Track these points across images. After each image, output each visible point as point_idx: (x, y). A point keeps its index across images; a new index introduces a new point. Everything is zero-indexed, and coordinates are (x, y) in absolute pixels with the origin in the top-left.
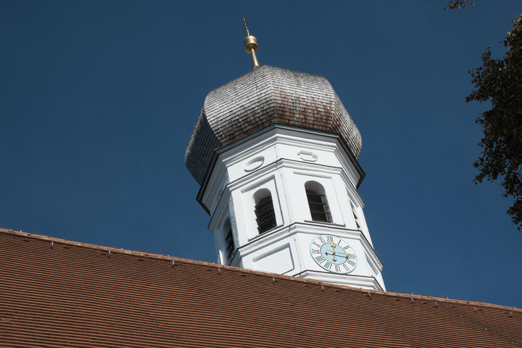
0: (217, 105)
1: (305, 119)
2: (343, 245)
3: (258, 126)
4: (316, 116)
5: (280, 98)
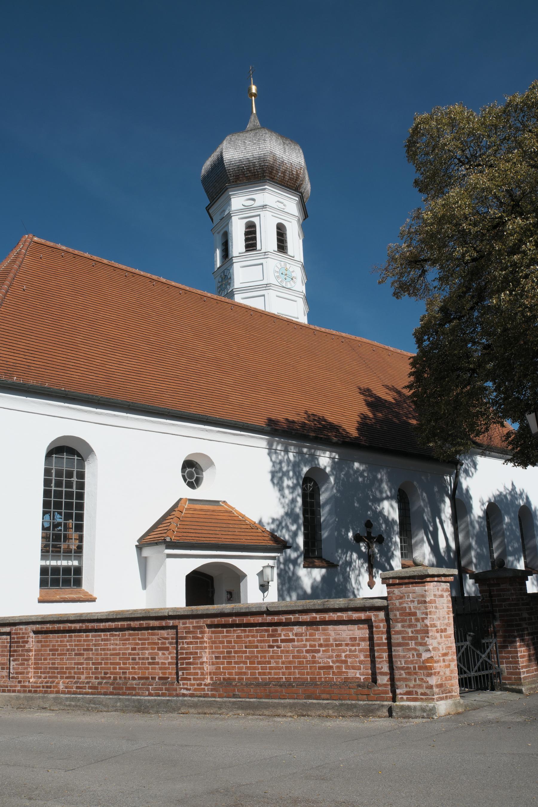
0: (232, 152)
1: (284, 177)
2: (291, 270)
3: (255, 175)
4: (291, 176)
5: (272, 160)
